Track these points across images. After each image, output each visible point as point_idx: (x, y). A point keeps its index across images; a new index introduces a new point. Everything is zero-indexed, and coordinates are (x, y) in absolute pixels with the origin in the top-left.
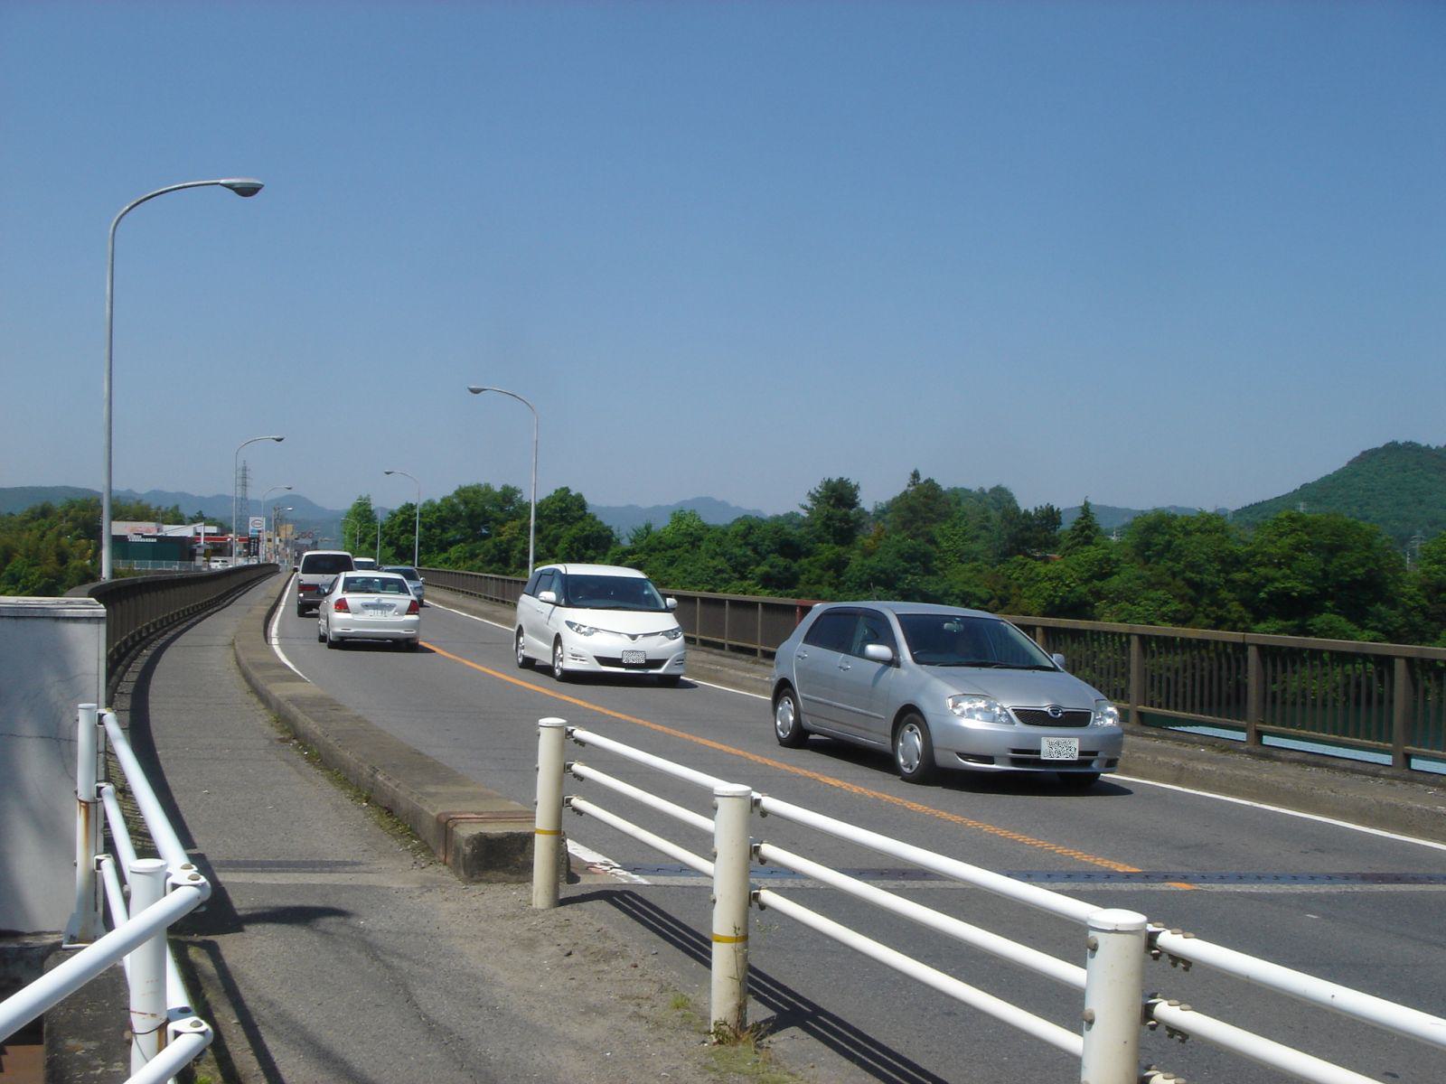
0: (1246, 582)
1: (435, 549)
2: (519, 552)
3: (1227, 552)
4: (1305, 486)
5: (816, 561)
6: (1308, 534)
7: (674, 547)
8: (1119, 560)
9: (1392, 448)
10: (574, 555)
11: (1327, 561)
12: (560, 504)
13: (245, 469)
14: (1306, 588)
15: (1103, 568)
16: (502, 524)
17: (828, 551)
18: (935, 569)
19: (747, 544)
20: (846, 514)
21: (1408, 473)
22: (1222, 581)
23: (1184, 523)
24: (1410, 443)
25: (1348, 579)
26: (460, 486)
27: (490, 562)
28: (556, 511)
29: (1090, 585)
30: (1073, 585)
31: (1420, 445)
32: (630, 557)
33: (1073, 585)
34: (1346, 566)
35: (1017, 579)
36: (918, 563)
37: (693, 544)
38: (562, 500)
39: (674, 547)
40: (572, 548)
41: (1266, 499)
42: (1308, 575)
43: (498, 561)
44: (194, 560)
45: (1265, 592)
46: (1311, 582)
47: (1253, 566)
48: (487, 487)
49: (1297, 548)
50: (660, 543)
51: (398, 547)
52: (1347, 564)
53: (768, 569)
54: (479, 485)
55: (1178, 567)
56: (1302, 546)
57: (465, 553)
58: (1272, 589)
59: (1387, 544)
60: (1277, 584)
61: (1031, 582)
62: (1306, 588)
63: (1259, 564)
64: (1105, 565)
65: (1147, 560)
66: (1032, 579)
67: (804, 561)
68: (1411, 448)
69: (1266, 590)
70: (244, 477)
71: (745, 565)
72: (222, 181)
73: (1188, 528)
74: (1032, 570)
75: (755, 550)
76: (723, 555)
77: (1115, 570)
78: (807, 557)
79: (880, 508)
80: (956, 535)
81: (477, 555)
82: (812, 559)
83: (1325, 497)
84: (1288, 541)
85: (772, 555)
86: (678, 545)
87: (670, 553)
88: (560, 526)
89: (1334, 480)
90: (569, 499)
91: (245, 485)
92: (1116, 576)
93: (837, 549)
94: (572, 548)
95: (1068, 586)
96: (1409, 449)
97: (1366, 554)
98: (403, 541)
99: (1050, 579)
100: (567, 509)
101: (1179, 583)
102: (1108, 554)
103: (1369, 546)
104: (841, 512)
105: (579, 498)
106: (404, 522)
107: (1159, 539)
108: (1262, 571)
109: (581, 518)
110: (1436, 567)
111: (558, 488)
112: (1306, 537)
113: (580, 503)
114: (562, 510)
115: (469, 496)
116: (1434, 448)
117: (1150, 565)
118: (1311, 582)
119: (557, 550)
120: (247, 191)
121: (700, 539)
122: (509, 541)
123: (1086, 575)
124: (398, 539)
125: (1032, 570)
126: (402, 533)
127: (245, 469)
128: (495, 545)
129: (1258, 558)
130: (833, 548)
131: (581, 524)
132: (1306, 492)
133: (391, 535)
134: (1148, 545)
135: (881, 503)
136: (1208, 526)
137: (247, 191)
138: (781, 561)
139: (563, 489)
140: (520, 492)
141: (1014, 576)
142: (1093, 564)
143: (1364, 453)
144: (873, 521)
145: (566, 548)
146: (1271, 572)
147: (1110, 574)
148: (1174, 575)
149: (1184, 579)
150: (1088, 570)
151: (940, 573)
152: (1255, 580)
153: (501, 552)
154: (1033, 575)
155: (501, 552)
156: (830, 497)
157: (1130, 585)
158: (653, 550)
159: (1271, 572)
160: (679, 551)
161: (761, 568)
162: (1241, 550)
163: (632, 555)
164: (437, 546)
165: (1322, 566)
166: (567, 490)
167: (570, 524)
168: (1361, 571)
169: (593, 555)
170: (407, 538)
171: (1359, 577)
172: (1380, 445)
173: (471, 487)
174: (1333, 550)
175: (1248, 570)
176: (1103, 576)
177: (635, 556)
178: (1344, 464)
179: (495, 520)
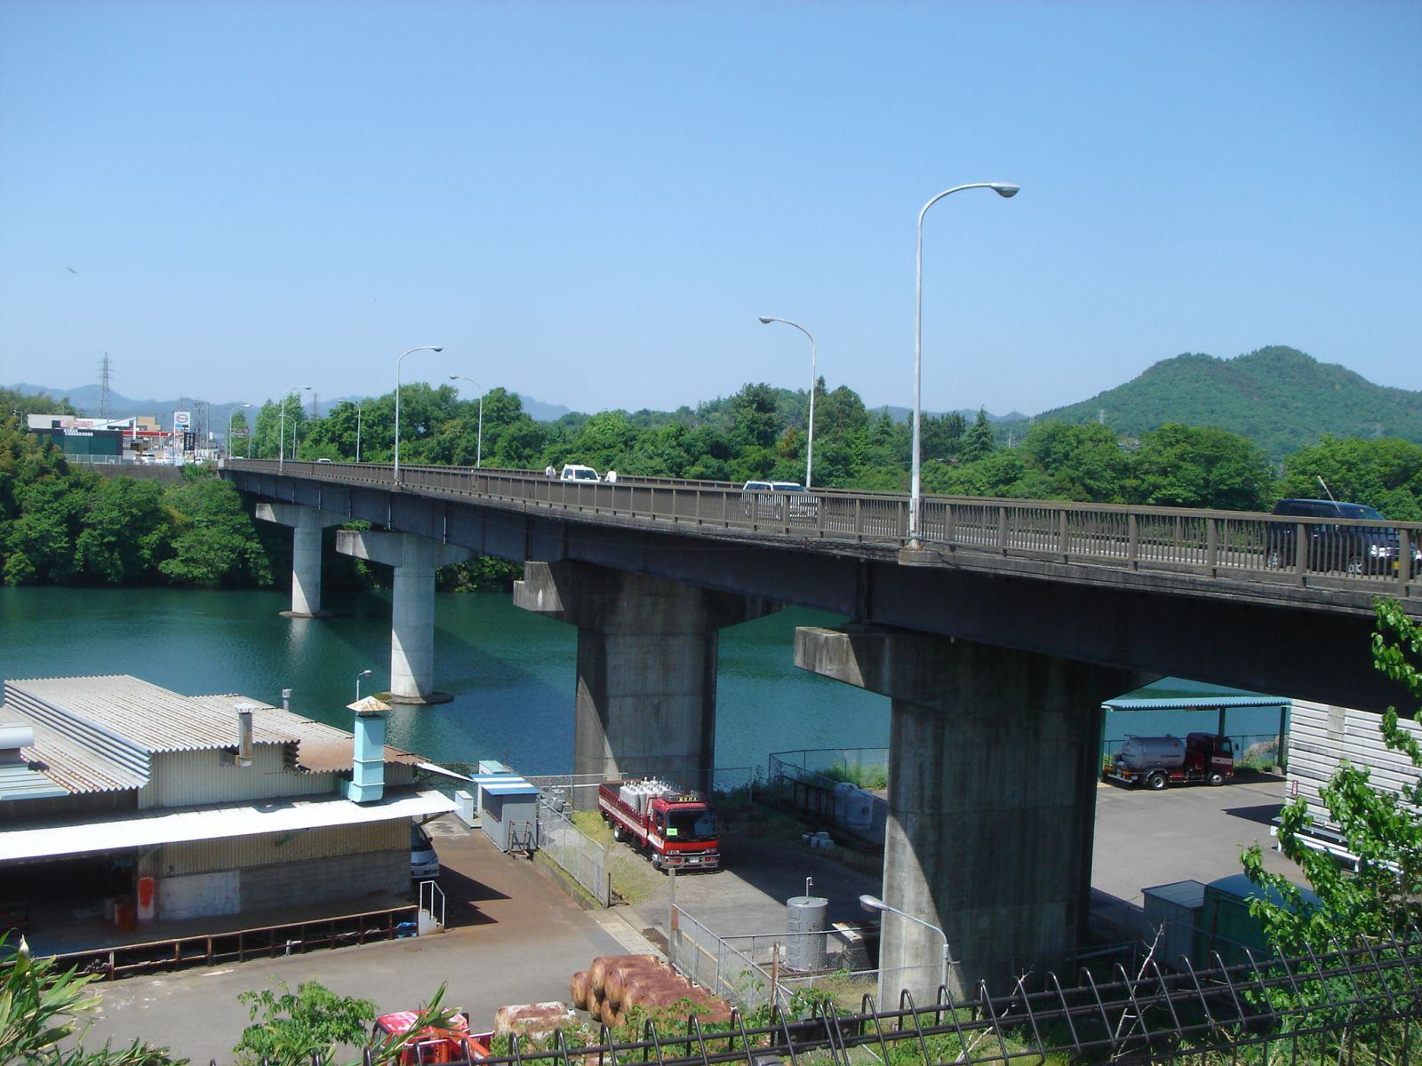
0: (1135, 489)
1: (378, 445)
2: (462, 450)
3: (1118, 460)
4: (1103, 394)
5: (744, 463)
6: (1193, 446)
7: (610, 447)
8: (1022, 467)
9: (1185, 359)
10: (513, 454)
11: (1209, 472)
12: (497, 404)
13: (106, 362)
14: (1190, 494)
15: (1007, 474)
16: (442, 422)
17: (754, 453)
18: (852, 471)
19: (679, 445)
20: (770, 418)
21: (1200, 384)
22: (1116, 487)
23: (1078, 433)
24: (1203, 355)
25: (1225, 488)
26: (719, 398)
27: (434, 460)
28: (493, 411)
29: (997, 490)
30: (982, 488)
31: (1210, 357)
32: (569, 456)
33: (982, 488)
34: (1225, 476)
35: (931, 482)
36: (840, 466)
37: (625, 443)
38: (499, 400)
39: (610, 447)
40: (511, 446)
41: (1065, 405)
42: (1191, 483)
43: (441, 459)
44: (122, 454)
45: (1154, 499)
46: (1194, 489)
47: (1142, 474)
48: (426, 386)
49: (1182, 458)
50: (595, 443)
51: (341, 443)
52: (1226, 474)
53: (703, 470)
54: (417, 385)
55: (1076, 474)
56: (1186, 456)
57: (409, 450)
58: (1160, 496)
59: (1262, 456)
60: (1164, 492)
61: (945, 485)
62: (1190, 494)
63: (1147, 472)
64: (1010, 471)
65: (1047, 467)
66: (945, 483)
67: (733, 462)
68: (1203, 359)
69: (1154, 496)
70: (106, 369)
71: (680, 466)
72: (994, 185)
73: (1081, 437)
74: (945, 474)
75: (687, 451)
76: (660, 455)
77: (1019, 476)
78: (735, 459)
79: (704, 407)
80: (857, 439)
81: (420, 454)
82: (739, 460)
83: (1124, 405)
84: (1178, 450)
85: (705, 456)
86: (612, 444)
87: (605, 452)
88: (498, 425)
89: (1131, 389)
90: (505, 400)
91: (106, 377)
92: (1019, 482)
93: (763, 451)
94: (511, 446)
95: (978, 489)
96: (1201, 360)
97: (1243, 464)
98: (346, 437)
99: (962, 483)
100: (504, 408)
101: (1079, 488)
102: (1014, 460)
103: (1245, 457)
104: (764, 416)
105: (515, 398)
106: (348, 420)
107: (1059, 448)
108: (1151, 478)
109: (518, 418)
110: (1301, 477)
111: (494, 388)
112: (1190, 449)
113: (516, 402)
114: (499, 410)
115: (409, 395)
116: (1224, 360)
117: (1050, 471)
118: (1194, 489)
119: (496, 448)
120: (1007, 193)
121: (634, 438)
122: (452, 440)
123: (993, 480)
124: (340, 436)
125: (945, 474)
126: (346, 430)
127: (106, 362)
128: (439, 443)
129: (1146, 466)
130: (760, 450)
131: (517, 424)
132: (1103, 399)
133: (334, 432)
134: (1048, 452)
135: (705, 403)
136: (1099, 436)
137: (1007, 193)
138: (714, 462)
139: (499, 389)
140: (457, 391)
141: (928, 479)
142: (999, 469)
143: (1158, 364)
144: (697, 419)
145: (506, 447)
146: (1161, 480)
147: (1015, 479)
148: (1072, 480)
149: (1084, 485)
150: (995, 475)
151: (857, 475)
152: (1145, 486)
153: (444, 449)
154: (946, 478)
155: (444, 449)
156: (753, 402)
157: (1034, 489)
158: (589, 449)
159: (1161, 480)
160: (615, 451)
161: (695, 468)
162: (1132, 459)
163: (571, 454)
164: (379, 443)
165: (1204, 475)
166: (502, 390)
167: (507, 423)
168: (1239, 480)
169: (530, 453)
170: (351, 436)
171: (1237, 486)
172: (1174, 356)
173: (411, 386)
174: (1211, 462)
175: (1136, 477)
176: (1009, 481)
177: (573, 455)
178: (1140, 373)
179: (436, 419)
